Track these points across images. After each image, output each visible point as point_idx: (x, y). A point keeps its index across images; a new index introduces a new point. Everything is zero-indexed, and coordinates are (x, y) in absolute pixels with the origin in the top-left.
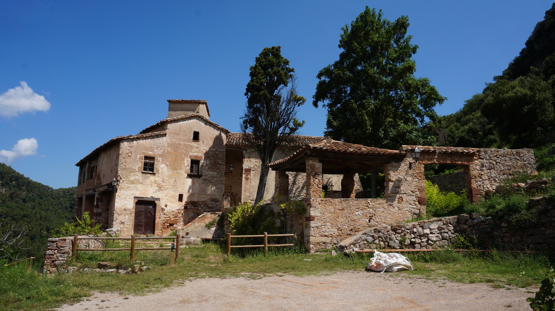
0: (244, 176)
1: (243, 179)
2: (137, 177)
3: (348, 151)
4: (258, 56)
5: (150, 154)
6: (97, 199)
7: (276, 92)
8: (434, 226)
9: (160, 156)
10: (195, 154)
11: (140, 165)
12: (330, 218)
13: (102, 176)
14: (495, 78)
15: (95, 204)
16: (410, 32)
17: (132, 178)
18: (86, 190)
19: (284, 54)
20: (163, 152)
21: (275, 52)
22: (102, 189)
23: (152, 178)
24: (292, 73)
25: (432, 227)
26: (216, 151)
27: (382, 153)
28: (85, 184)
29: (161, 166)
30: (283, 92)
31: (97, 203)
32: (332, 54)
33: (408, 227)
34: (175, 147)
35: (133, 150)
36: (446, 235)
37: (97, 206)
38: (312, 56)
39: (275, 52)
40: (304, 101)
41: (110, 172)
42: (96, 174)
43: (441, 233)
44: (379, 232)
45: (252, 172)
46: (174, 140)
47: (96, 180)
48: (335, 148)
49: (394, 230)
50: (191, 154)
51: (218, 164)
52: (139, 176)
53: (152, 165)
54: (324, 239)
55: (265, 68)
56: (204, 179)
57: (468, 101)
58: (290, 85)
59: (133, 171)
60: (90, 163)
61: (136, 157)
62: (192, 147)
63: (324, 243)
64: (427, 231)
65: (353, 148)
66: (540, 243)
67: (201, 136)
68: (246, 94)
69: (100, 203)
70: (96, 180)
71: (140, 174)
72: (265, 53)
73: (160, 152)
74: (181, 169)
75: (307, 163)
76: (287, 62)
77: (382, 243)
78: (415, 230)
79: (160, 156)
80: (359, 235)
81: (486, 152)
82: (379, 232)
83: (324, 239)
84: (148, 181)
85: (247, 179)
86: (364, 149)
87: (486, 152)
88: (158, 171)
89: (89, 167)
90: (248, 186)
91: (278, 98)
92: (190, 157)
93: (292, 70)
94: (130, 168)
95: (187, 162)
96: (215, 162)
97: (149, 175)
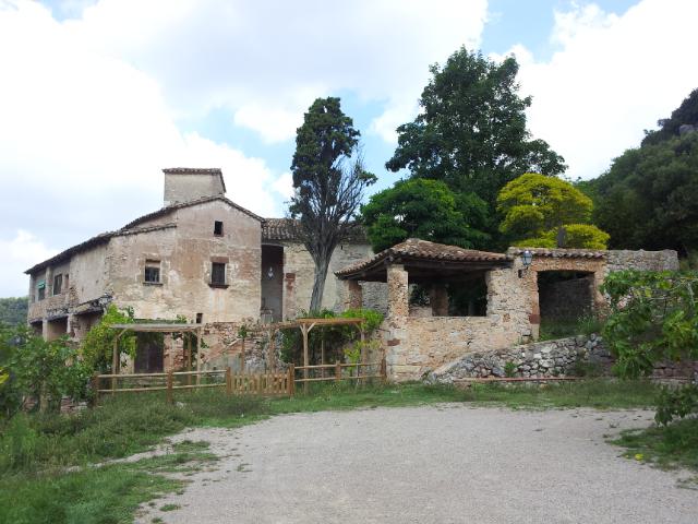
0: (285, 284)
1: (285, 289)
2: (136, 290)
3: (441, 257)
4: (308, 112)
5: (154, 255)
6: (72, 323)
7: (335, 164)
8: (547, 350)
9: (168, 258)
10: (218, 255)
11: (140, 272)
12: (416, 339)
13: (78, 289)
14: (660, 122)
15: (69, 330)
16: (518, 79)
17: (129, 292)
18: (48, 311)
19: (345, 109)
20: (173, 253)
21: (333, 104)
22: (80, 309)
23: (158, 291)
24: (357, 137)
25: (544, 350)
26: (248, 249)
27: (483, 258)
28: (46, 301)
29: (170, 274)
30: (344, 164)
31: (72, 330)
32: (410, 109)
33: (514, 351)
34: (189, 245)
35: (128, 250)
36: (560, 360)
37: (73, 335)
38: (386, 116)
39: (333, 104)
40: (375, 179)
41: (93, 282)
42: (67, 287)
43: (554, 358)
44: (480, 357)
45: (297, 278)
46: (188, 235)
47: (67, 295)
48: (424, 252)
49: (499, 354)
50: (212, 255)
51: (251, 268)
52: (139, 289)
53: (156, 271)
54: (412, 368)
55: (317, 130)
56: (232, 291)
57: (616, 160)
58: (354, 154)
59: (131, 282)
60: (52, 270)
61: (134, 261)
62: (213, 245)
63: (412, 373)
64: (538, 356)
65: (447, 251)
66: (663, 368)
67: (225, 228)
68: (292, 168)
69: (76, 330)
70: (67, 295)
71: (140, 286)
72: (318, 106)
73: (169, 253)
74: (198, 277)
75: (389, 272)
76: (350, 122)
77: (484, 370)
78: (523, 354)
79: (168, 258)
80: (457, 360)
81: (617, 256)
82: (480, 357)
83: (412, 368)
84: (153, 295)
85: (289, 288)
86: (461, 252)
87: (617, 256)
88: (165, 280)
89: (51, 276)
90: (292, 299)
91: (337, 175)
92: (212, 258)
93: (358, 133)
94: (125, 278)
95: (207, 267)
96: (247, 265)
97: (153, 287)
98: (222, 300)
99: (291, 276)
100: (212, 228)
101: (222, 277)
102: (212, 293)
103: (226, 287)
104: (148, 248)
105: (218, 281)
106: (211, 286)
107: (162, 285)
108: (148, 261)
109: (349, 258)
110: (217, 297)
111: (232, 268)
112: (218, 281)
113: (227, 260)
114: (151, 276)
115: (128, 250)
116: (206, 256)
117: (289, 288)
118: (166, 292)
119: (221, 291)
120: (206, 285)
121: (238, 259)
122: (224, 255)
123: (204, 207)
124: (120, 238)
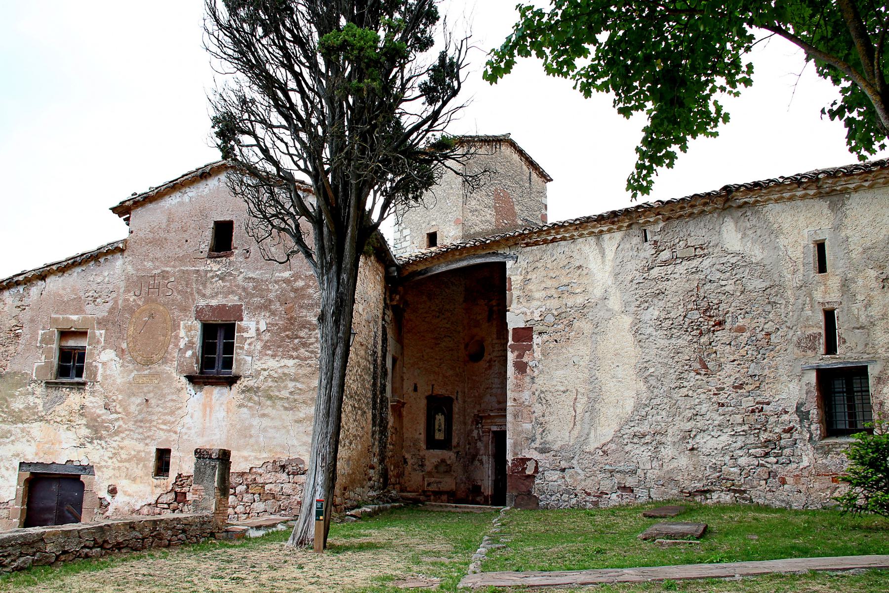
0: (511, 357)
1: (511, 370)
2: (31, 399)
5: (75, 319)
10: (214, 302)
17: (18, 405)
26: (297, 277)
29: (104, 361)
35: (25, 316)
45: (537, 340)
46: (149, 264)
50: (202, 303)
53: (81, 355)
56: (248, 390)
61: (34, 336)
62: (203, 279)
71: (40, 390)
74: (165, 360)
79: (102, 323)
84: (61, 410)
85: (521, 367)
90: (526, 395)
92: (199, 313)
95: (189, 334)
97: (65, 391)
98: (220, 414)
99: (525, 334)
100: (208, 235)
101: (208, 347)
102: (195, 400)
103: (231, 381)
104: (63, 305)
105: (215, 361)
106: (191, 379)
107: (84, 384)
108: (65, 334)
109: (665, 263)
110: (207, 408)
111: (251, 327)
112: (215, 361)
113: (237, 312)
114: (70, 366)
115: (25, 316)
116: (184, 309)
117: (521, 367)
118: (91, 400)
119: (218, 394)
120: (184, 380)
121: (265, 307)
122: (232, 300)
123: (192, 193)
124: (13, 291)
